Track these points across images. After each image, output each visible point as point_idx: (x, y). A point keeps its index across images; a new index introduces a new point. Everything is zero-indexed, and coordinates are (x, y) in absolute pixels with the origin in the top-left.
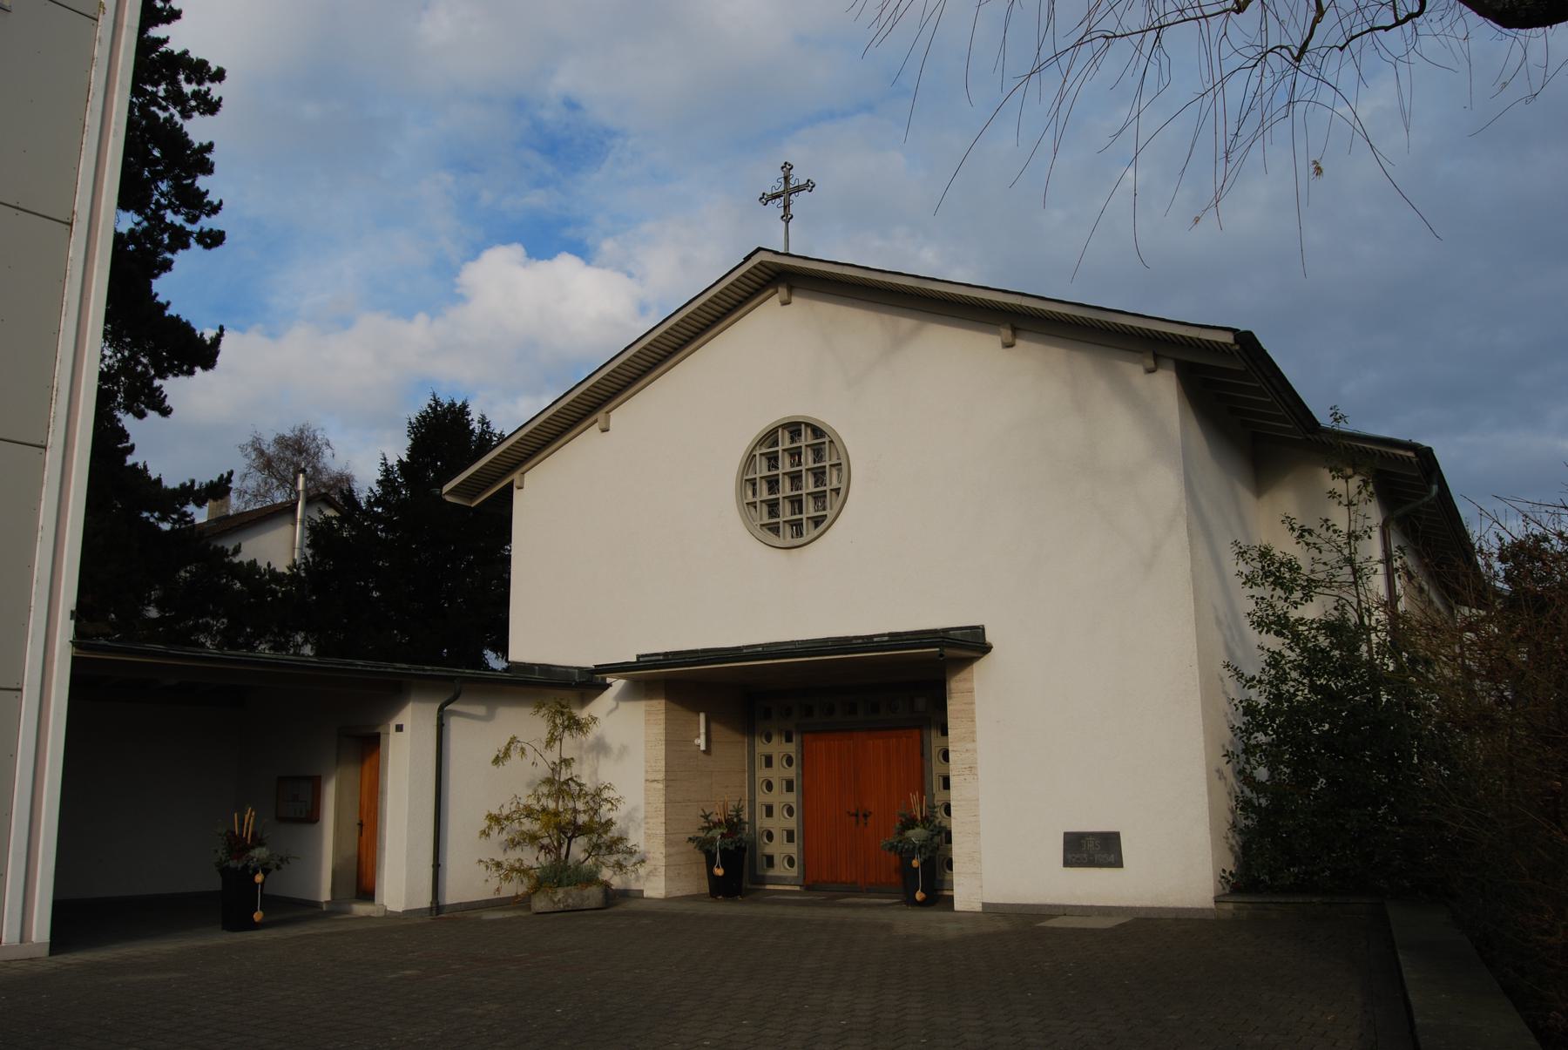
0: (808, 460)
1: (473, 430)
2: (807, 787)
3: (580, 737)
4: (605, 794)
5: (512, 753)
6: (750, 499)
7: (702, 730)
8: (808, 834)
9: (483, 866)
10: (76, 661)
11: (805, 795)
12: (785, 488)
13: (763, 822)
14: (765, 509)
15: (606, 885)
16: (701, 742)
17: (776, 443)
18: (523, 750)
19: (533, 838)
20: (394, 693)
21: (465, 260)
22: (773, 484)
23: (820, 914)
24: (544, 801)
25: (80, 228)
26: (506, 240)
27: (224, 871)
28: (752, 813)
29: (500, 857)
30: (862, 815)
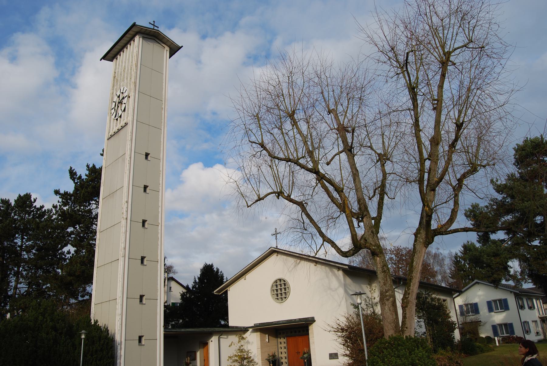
0: (283, 286)
2: (288, 348)
7: (267, 338)
11: (288, 349)
12: (279, 292)
13: (280, 355)
14: (276, 295)
16: (267, 340)
17: (277, 283)
18: (234, 344)
19: (237, 360)
20: (210, 335)
21: (183, 169)
22: (277, 290)
24: (238, 353)
25: (159, 262)
26: (196, 161)
28: (278, 354)
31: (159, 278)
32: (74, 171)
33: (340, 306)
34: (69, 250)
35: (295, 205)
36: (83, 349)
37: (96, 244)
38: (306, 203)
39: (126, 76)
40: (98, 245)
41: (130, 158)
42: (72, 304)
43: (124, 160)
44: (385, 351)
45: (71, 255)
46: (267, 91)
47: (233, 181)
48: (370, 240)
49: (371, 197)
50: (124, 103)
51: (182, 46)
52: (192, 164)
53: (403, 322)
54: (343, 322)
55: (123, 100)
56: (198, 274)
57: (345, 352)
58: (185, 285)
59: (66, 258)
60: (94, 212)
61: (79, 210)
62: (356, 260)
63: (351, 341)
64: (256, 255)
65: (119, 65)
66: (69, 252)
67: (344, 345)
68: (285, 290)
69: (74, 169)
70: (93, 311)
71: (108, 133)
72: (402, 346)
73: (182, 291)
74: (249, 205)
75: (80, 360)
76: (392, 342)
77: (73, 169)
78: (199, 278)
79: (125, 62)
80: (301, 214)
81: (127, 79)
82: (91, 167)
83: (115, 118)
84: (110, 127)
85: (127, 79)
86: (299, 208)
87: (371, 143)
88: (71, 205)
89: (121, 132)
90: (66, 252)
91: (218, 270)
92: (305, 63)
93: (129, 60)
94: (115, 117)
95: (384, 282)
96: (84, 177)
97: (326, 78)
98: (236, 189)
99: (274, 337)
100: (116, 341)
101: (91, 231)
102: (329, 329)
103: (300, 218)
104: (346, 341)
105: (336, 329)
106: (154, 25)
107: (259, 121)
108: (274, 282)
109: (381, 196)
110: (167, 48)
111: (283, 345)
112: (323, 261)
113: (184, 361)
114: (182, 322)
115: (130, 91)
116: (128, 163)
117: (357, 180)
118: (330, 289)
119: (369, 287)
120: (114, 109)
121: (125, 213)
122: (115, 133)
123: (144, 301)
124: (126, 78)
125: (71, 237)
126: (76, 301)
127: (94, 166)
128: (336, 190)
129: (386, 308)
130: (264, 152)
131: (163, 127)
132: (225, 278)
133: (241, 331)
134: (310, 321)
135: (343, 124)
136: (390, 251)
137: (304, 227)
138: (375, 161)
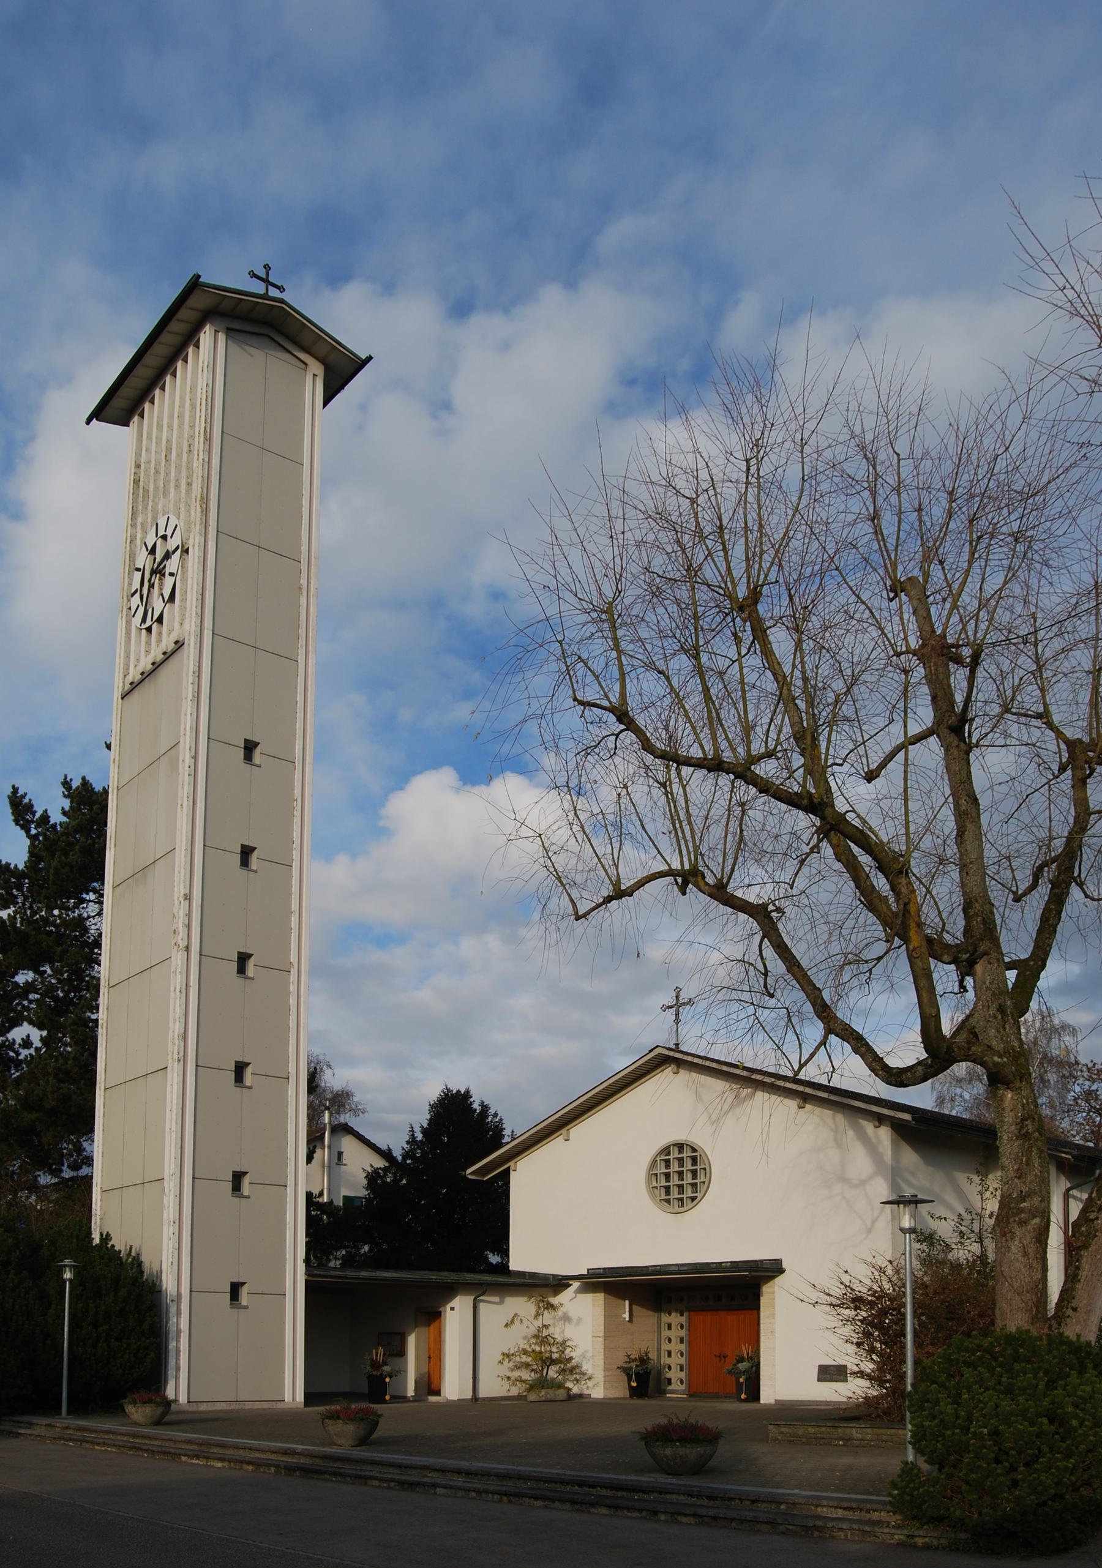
0: (688, 1165)
1: (475, 1110)
2: (691, 1341)
3: (553, 1313)
4: (568, 1343)
5: (515, 1321)
6: (654, 1184)
7: (627, 1309)
8: (691, 1367)
9: (500, 1379)
10: (308, 1283)
12: (675, 1180)
13: (665, 1360)
14: (663, 1190)
15: (569, 1389)
16: (626, 1316)
17: (669, 1154)
18: (521, 1320)
19: (527, 1365)
20: (450, 1291)
22: (667, 1176)
23: (693, 1404)
24: (533, 1346)
25: (292, 1079)
26: (434, 763)
27: (370, 1377)
29: (509, 1374)
30: (723, 1357)
31: (291, 1127)
32: (26, 801)
33: (869, 1231)
34: (28, 1036)
35: (743, 916)
36: (70, 1307)
37: (100, 1022)
38: (779, 910)
39: (173, 474)
40: (105, 1025)
41: (195, 757)
42: (47, 1186)
43: (174, 765)
44: (967, 1372)
45: (32, 1051)
46: (661, 516)
47: (531, 833)
48: (991, 1035)
49: (1020, 892)
50: (171, 574)
51: (370, 358)
52: (420, 772)
53: (1066, 1293)
54: (863, 1280)
55: (168, 563)
56: (422, 1118)
57: (857, 1365)
58: (384, 1147)
59: (20, 1058)
60: (93, 927)
61: (47, 918)
62: (961, 1096)
63: (884, 1334)
64: (621, 1062)
65: (149, 438)
66: (27, 1043)
67: (858, 1345)
68: (695, 1176)
69: (26, 794)
70: (98, 1209)
71: (121, 676)
72: (1029, 1362)
73: (371, 1166)
74: (580, 913)
75: (63, 1335)
76: (997, 1349)
77: (21, 792)
78: (424, 1131)
79: (170, 427)
80: (760, 946)
81: (177, 486)
82: (77, 788)
83: (144, 626)
84: (128, 656)
85: (177, 486)
86: (752, 924)
87: (1045, 705)
88: (24, 904)
89: (165, 673)
90: (19, 1041)
91: (485, 1108)
92: (815, 403)
93: (181, 417)
94: (144, 620)
95: (1018, 1169)
96: (56, 818)
97: (895, 462)
98: (542, 861)
99: (648, 1309)
100: (164, 1294)
101: (88, 981)
102: (815, 1296)
103: (754, 957)
104: (867, 1335)
105: (838, 1298)
106: (266, 281)
107: (614, 628)
108: (660, 1153)
109: (1056, 891)
110: (316, 368)
111: (676, 1333)
112: (824, 1095)
113: (367, 1357)
114: (370, 1250)
115: (189, 530)
116: (187, 774)
117: (969, 835)
118: (843, 1179)
119: (976, 1179)
120: (138, 594)
121: (182, 930)
122: (146, 676)
123: (246, 1189)
124: (172, 484)
125: (27, 999)
126: (55, 1180)
127: (85, 783)
128: (881, 868)
129: (1015, 1247)
130: (629, 737)
131: (302, 651)
132: (507, 1132)
133: (546, 1286)
134: (773, 1269)
135: (944, 636)
136: (1089, 1070)
137: (765, 986)
138: (1055, 768)
